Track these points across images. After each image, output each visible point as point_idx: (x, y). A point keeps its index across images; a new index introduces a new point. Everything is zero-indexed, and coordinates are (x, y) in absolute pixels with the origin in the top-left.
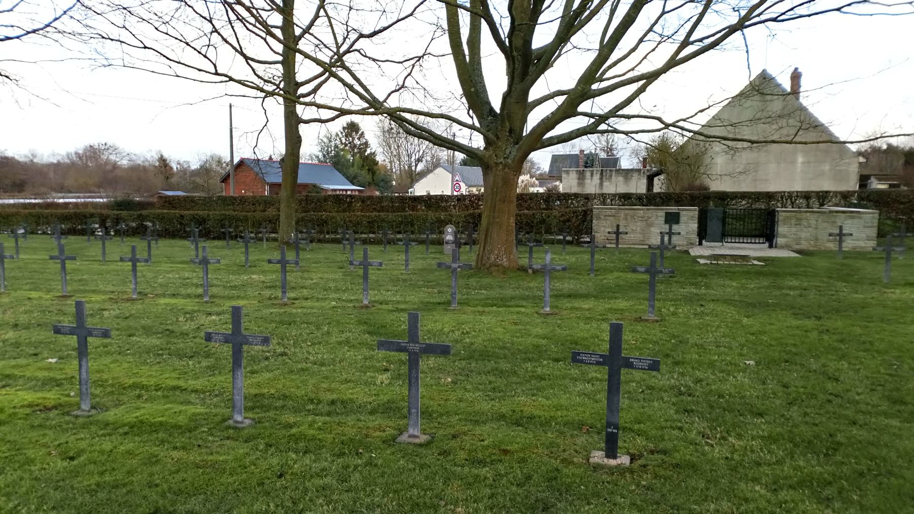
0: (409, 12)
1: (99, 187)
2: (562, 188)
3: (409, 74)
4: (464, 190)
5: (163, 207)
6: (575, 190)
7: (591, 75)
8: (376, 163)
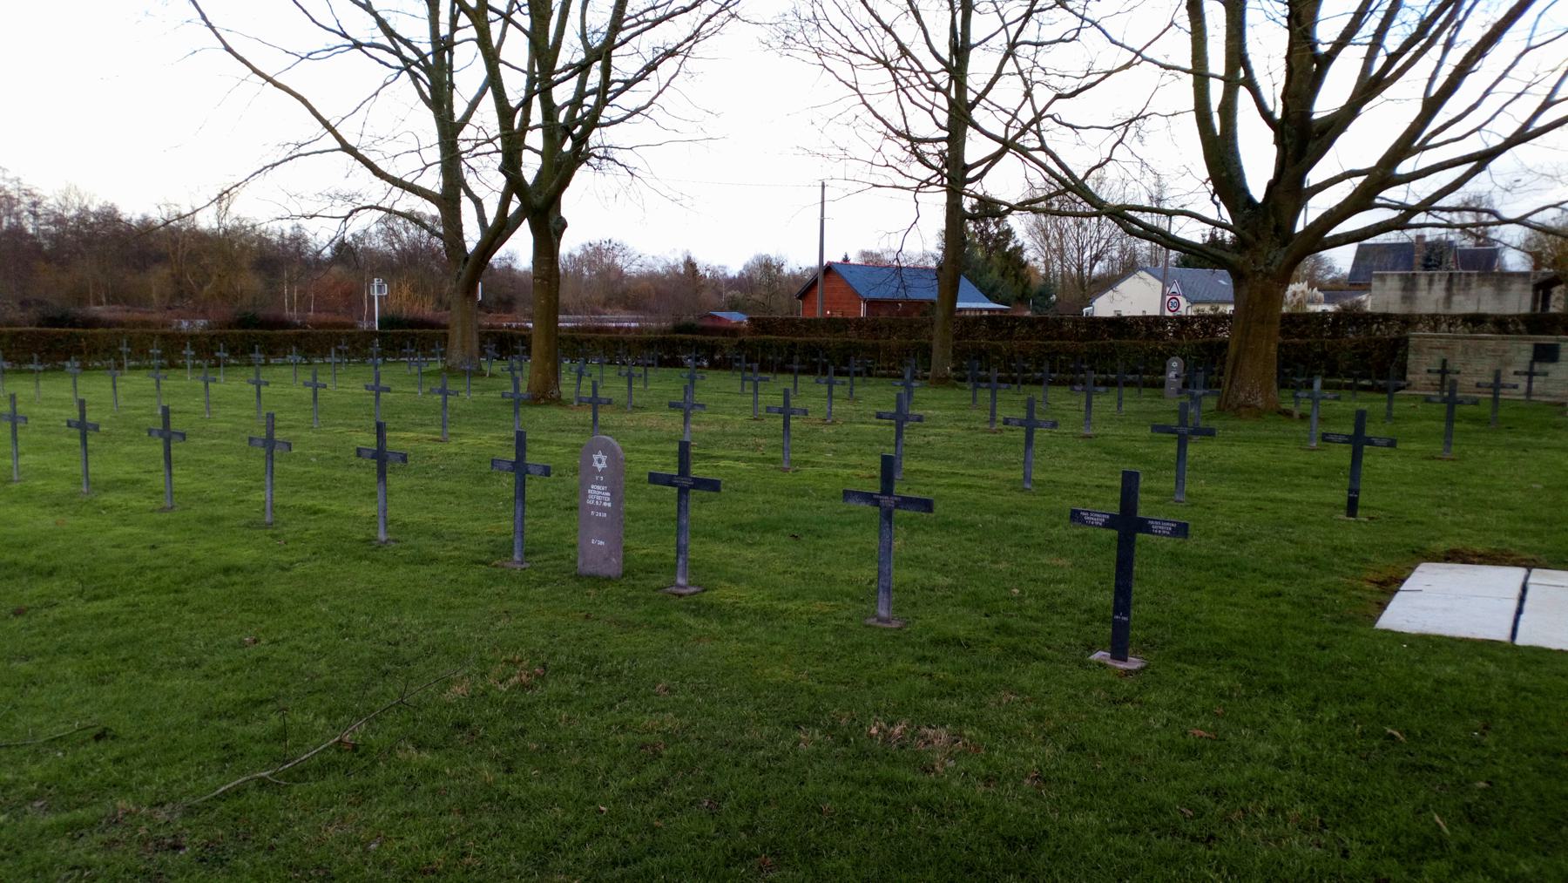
0: (1115, 38)
1: (605, 305)
2: (1367, 303)
3: (1120, 141)
4: (1185, 309)
5: (755, 332)
6: (1396, 308)
7: (1405, 146)
8: (1024, 265)
